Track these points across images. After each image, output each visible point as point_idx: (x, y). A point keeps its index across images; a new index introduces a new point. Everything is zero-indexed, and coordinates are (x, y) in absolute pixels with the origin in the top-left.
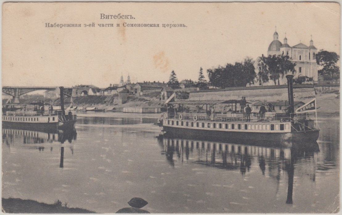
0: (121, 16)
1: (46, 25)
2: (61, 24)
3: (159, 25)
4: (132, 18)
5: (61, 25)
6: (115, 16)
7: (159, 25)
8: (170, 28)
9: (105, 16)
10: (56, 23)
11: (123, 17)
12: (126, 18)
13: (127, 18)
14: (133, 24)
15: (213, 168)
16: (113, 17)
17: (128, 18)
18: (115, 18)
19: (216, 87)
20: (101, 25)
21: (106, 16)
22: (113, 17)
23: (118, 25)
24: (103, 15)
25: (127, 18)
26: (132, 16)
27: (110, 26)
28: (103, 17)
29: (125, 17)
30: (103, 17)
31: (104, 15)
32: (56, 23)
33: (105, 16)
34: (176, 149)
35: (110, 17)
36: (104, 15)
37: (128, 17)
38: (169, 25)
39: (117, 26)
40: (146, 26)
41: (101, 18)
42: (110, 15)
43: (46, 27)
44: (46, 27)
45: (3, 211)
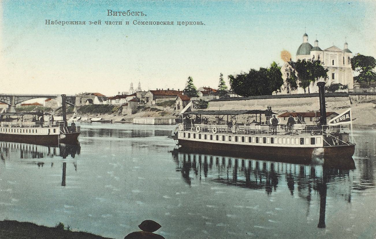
9: (113, 13)
11: (133, 14)
16: (121, 14)
20: (108, 23)
22: (121, 14)
24: (110, 11)
27: (118, 23)
28: (110, 14)
30: (110, 14)
31: (112, 11)
33: (113, 13)
35: (118, 14)
36: (112, 11)
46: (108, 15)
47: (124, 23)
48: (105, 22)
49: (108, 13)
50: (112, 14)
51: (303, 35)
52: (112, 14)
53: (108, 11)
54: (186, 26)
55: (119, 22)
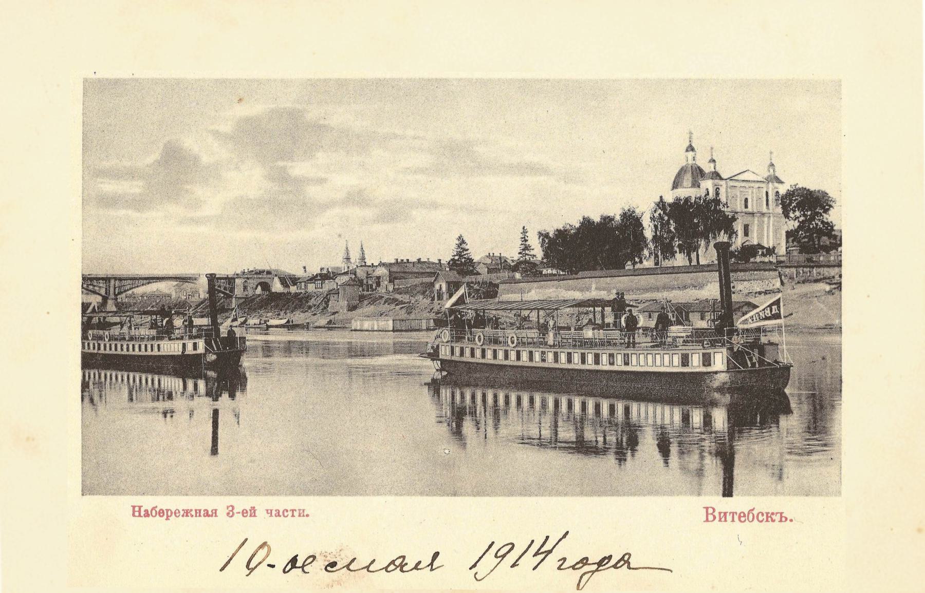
0: (173, 514)
2: (200, 518)
4: (783, 519)
9: (716, 514)
10: (753, 510)
11: (761, 518)
12: (767, 521)
13: (770, 519)
16: (736, 517)
21: (720, 513)
22: (736, 517)
24: (710, 511)
25: (770, 519)
27: (296, 514)
28: (711, 518)
29: (765, 517)
30: (711, 518)
32: (753, 510)
33: (716, 514)
35: (729, 518)
37: (774, 517)
38: (282, 516)
39: (218, 512)
42: (730, 513)
46: (707, 520)
48: (267, 510)
49: (707, 514)
50: (715, 518)
51: (217, 518)
52: (715, 518)
53: (707, 512)
55: (298, 511)
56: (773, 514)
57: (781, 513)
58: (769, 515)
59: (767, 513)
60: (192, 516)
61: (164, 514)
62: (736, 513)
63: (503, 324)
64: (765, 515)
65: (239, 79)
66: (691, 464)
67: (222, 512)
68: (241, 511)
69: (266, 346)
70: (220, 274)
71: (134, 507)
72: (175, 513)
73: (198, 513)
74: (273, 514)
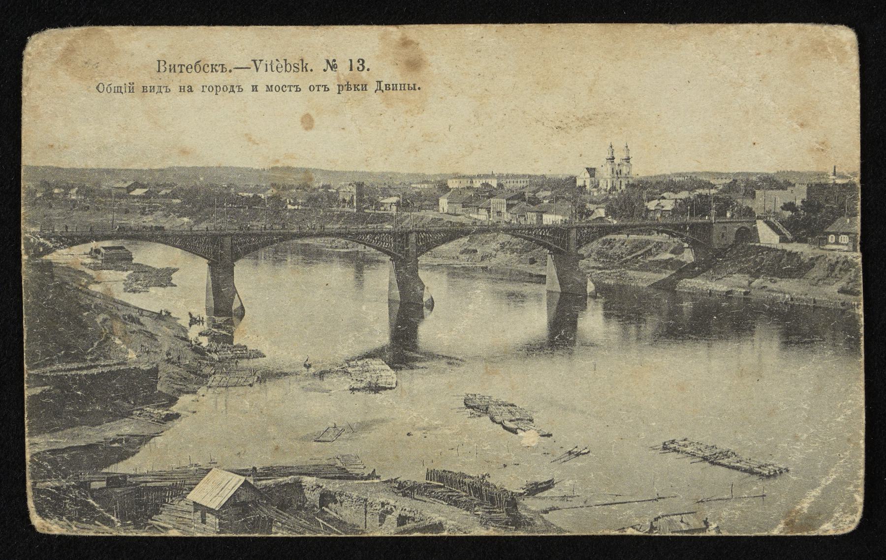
0: (222, 89)
1: (181, 89)
3: (256, 86)
5: (216, 86)
6: (190, 67)
7: (256, 86)
8: (216, 94)
11: (207, 69)
12: (212, 71)
14: (272, 86)
15: (437, 276)
16: (184, 69)
17: (216, 70)
18: (189, 70)
19: (607, 215)
22: (184, 69)
23: (255, 88)
24: (162, 63)
26: (224, 66)
30: (162, 69)
34: (747, 299)
37: (217, 68)
38: (214, 86)
39: (367, 87)
40: (147, 92)
41: (159, 71)
42: (179, 65)
43: (180, 91)
44: (180, 91)
45: (431, 306)
47: (197, 89)
54: (216, 94)
56: (216, 65)
57: (223, 65)
58: (214, 66)
59: (212, 65)
60: (359, 90)
61: (213, 89)
62: (184, 65)
63: (333, 349)
64: (210, 66)
65: (732, 187)
66: (837, 33)
67: (247, 88)
68: (186, 66)
69: (110, 511)
70: (208, 276)
71: (181, 87)
72: (223, 88)
73: (224, 89)
74: (149, 88)
